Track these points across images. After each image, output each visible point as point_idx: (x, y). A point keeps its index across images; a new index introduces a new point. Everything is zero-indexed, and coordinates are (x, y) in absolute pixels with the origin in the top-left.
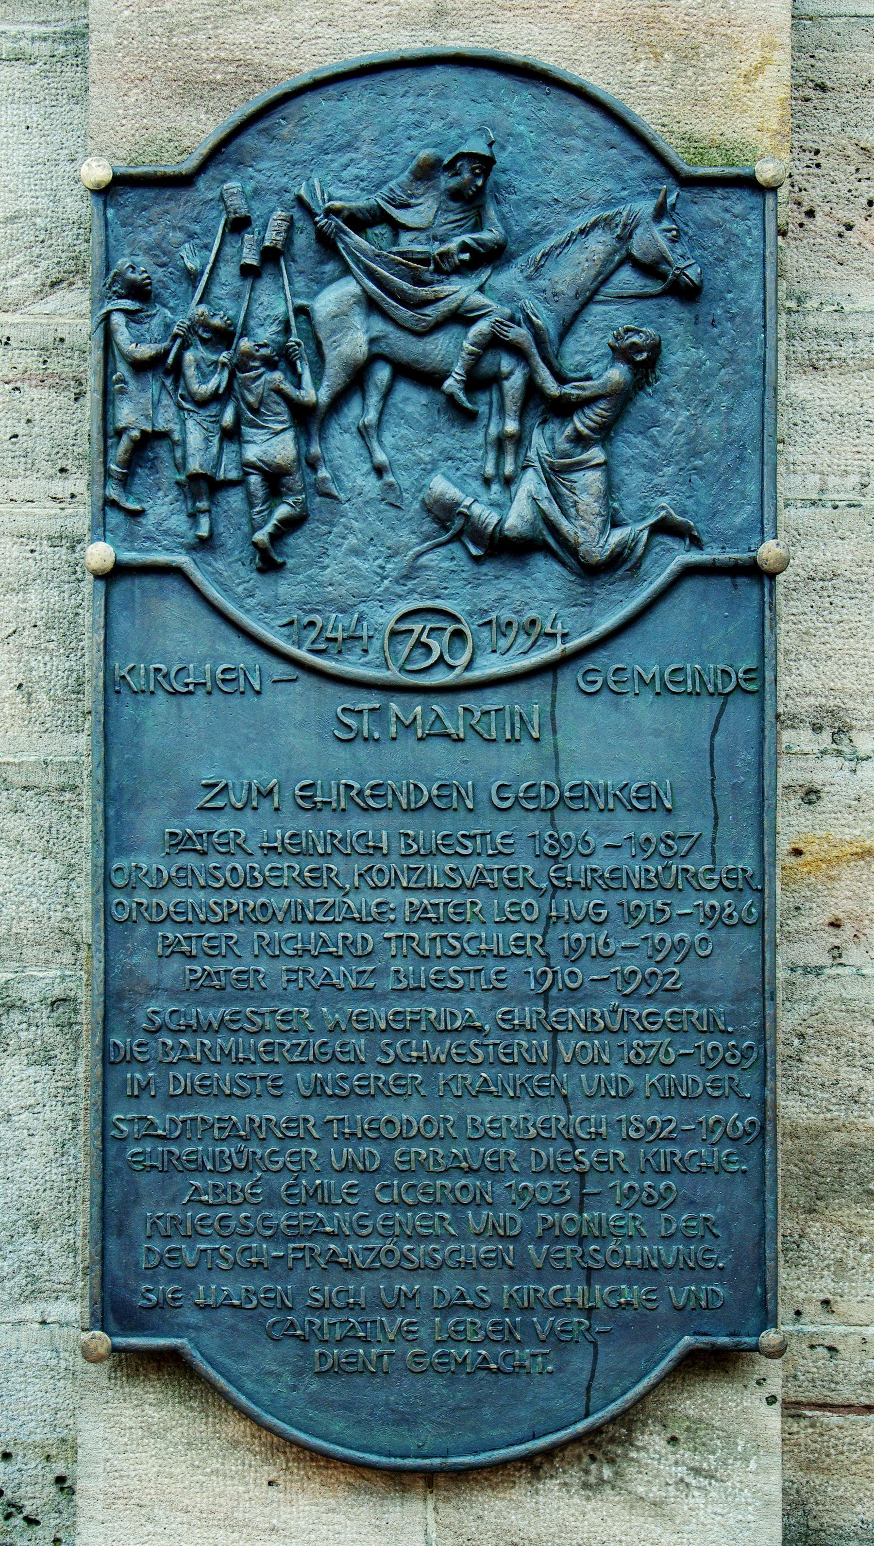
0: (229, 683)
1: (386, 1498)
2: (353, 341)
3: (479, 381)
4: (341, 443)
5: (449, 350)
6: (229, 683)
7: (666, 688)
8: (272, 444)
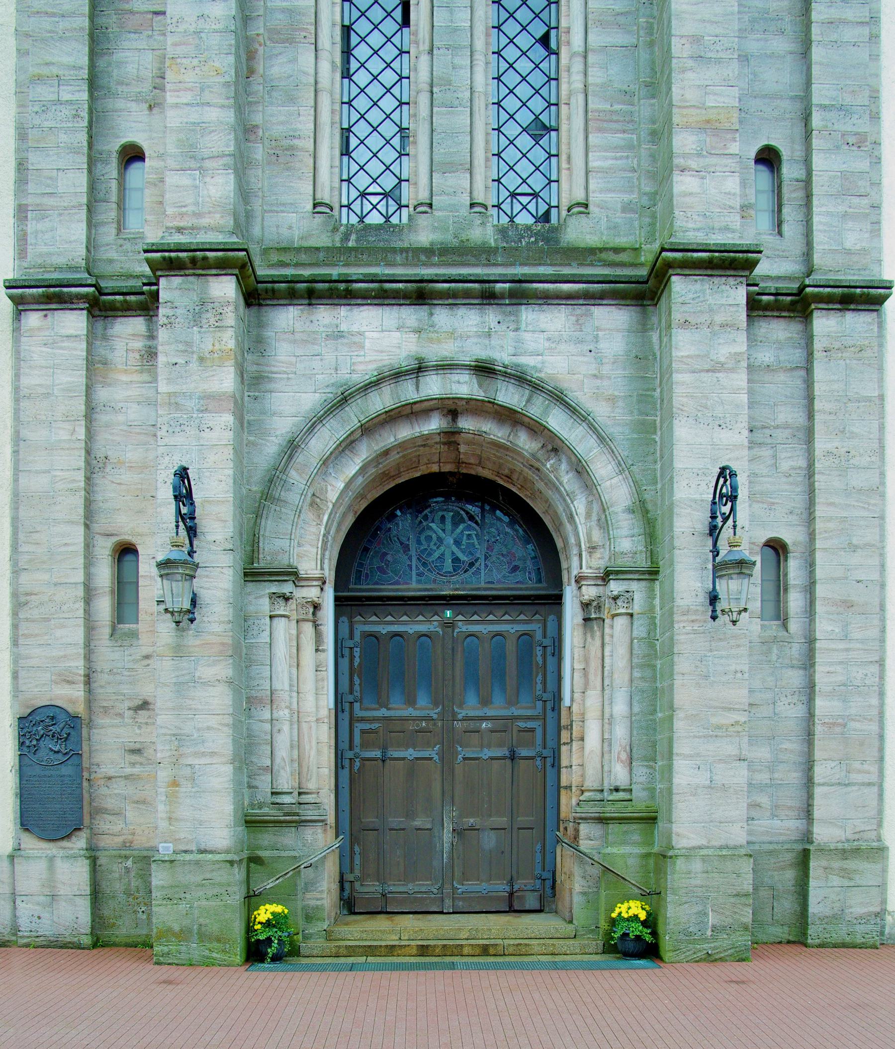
0: (31, 765)
1: (796, 895)
2: (42, 732)
3: (53, 736)
4: (41, 742)
5: (51, 733)
6: (31, 765)
7: (71, 765)
8: (34, 742)
